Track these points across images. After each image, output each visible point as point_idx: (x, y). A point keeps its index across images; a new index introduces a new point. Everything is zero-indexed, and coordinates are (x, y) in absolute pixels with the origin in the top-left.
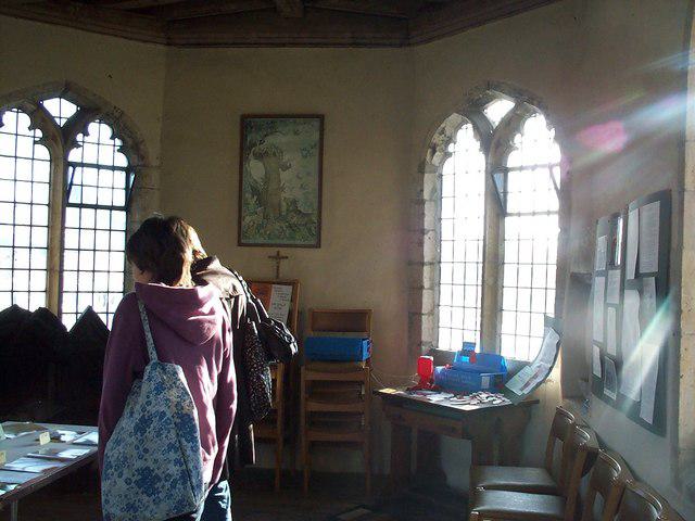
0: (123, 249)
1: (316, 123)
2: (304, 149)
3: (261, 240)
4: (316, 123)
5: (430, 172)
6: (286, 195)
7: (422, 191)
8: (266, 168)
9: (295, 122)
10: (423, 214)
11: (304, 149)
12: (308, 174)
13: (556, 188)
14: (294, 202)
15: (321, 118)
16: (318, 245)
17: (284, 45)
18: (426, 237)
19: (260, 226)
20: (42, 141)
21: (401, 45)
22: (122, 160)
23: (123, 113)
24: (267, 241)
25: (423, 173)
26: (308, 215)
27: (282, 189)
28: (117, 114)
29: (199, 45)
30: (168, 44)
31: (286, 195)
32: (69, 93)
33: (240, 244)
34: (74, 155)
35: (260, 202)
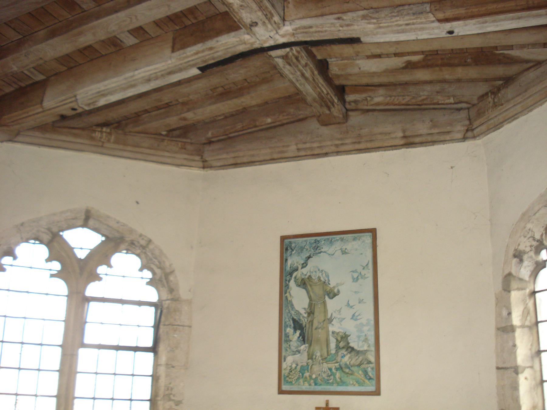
0: (76, 401)
1: (367, 239)
2: (355, 271)
3: (305, 387)
4: (367, 239)
5: (519, 289)
6: (334, 327)
7: (510, 314)
8: (310, 297)
9: (342, 240)
10: (515, 346)
11: (355, 271)
12: (361, 301)
13: (496, 48)
14: (345, 337)
15: (373, 232)
16: (377, 392)
17: (326, 154)
18: (522, 378)
19: (303, 370)
20: (59, 275)
21: (464, 139)
22: (152, 295)
23: (150, 241)
24: (313, 388)
25: (509, 292)
26: (365, 352)
27: (330, 321)
28: (143, 242)
29: (236, 165)
30: (204, 168)
31: (334, 327)
32: (328, 290)
33: (281, 392)
34: (92, 289)
35: (303, 339)
